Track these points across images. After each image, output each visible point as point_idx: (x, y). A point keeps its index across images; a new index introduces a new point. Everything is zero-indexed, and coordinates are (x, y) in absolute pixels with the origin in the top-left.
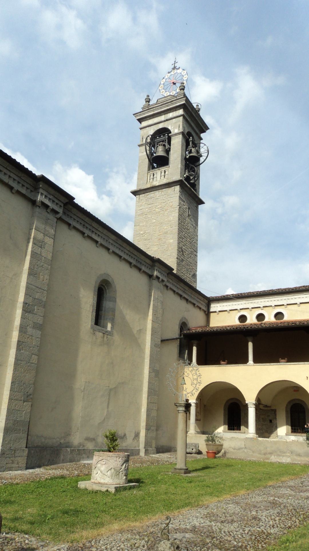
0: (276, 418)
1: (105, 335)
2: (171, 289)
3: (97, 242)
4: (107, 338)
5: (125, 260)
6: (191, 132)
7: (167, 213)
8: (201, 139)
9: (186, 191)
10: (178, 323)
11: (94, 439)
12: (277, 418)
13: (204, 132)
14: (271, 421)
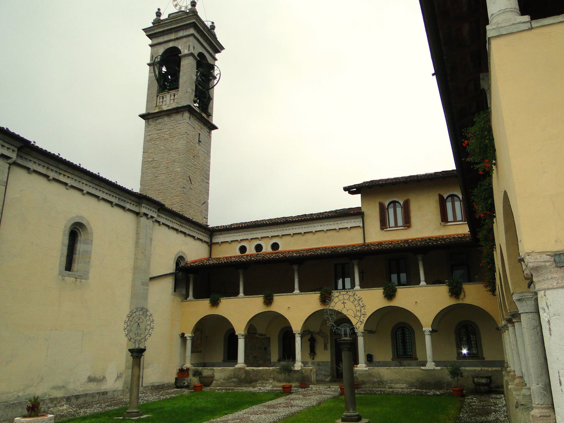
1: (77, 279)
2: (163, 224)
3: (66, 184)
4: (81, 282)
5: (103, 199)
6: (203, 52)
7: (175, 140)
9: (195, 116)
10: (173, 258)
11: (64, 387)
13: (219, 52)
14: (265, 349)
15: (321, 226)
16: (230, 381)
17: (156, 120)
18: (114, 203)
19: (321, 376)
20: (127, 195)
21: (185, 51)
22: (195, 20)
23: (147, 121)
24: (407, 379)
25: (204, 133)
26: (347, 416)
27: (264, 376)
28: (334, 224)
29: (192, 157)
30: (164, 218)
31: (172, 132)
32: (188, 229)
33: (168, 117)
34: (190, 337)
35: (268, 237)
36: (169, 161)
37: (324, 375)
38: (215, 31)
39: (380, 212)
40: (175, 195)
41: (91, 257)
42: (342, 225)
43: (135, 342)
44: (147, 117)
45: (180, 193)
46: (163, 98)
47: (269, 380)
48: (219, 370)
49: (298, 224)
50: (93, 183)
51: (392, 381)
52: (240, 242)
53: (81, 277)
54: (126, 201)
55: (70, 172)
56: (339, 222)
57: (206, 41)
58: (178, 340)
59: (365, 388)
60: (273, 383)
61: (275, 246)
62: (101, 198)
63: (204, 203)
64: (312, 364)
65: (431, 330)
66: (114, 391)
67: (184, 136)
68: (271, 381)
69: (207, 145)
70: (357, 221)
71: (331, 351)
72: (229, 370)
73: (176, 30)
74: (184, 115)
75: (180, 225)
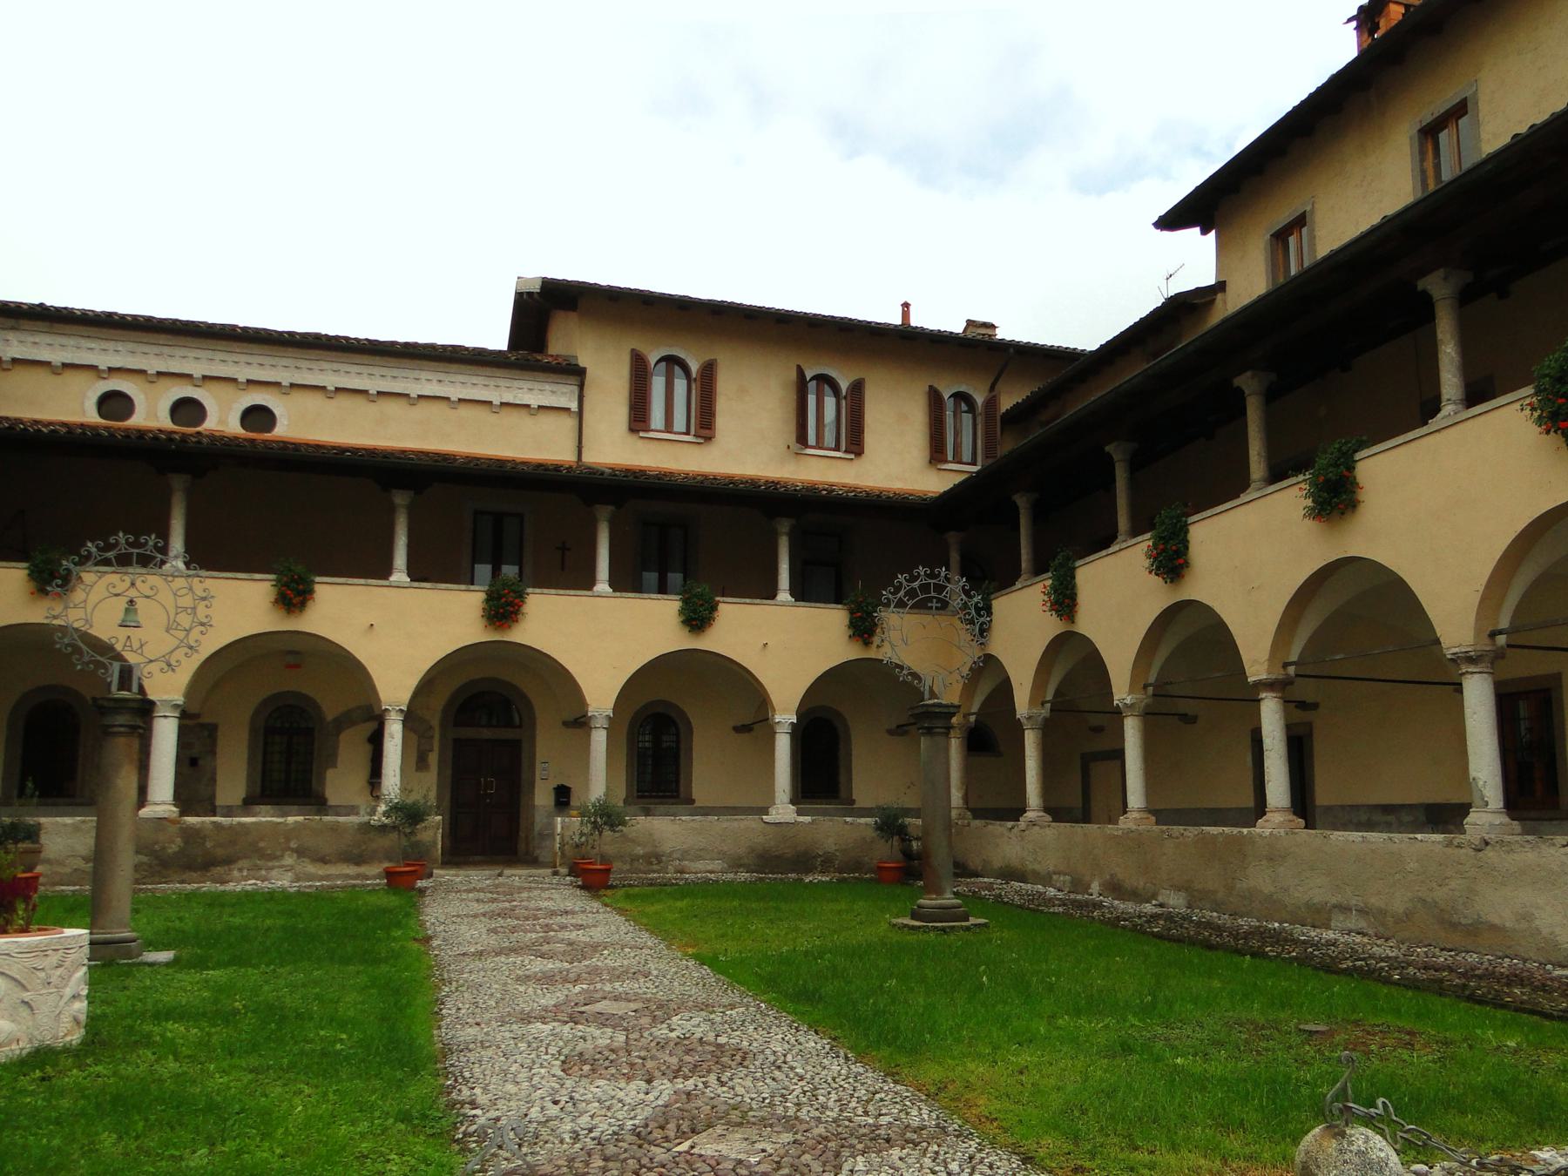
0: (213, 752)
12: (218, 750)
15: (440, 381)
24: (725, 848)
27: (262, 844)
39: (631, 379)
47: (282, 856)
51: (685, 855)
52: (105, 376)
56: (502, 382)
61: (258, 416)
65: (795, 721)
68: (289, 860)
70: (562, 393)
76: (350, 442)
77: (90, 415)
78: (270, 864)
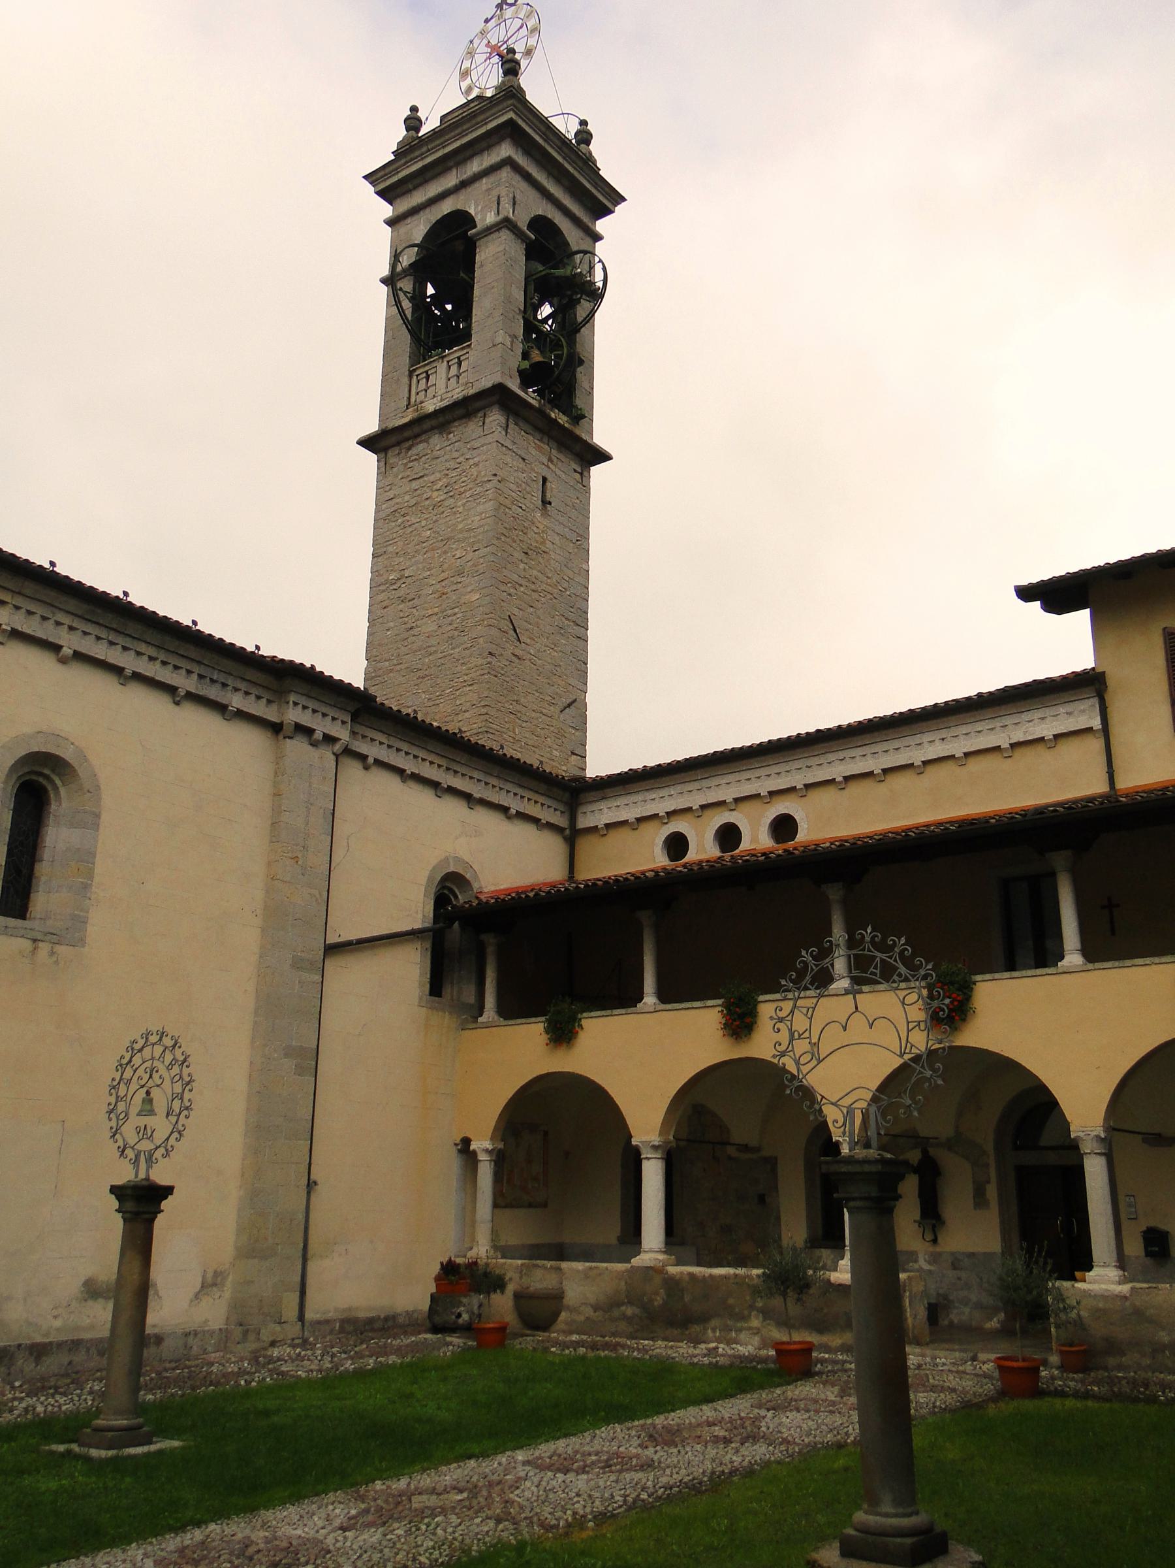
1: (41, 944)
2: (379, 763)
4: (52, 953)
5: (138, 677)
7: (464, 505)
8: (597, 237)
9: (527, 421)
10: (424, 881)
14: (762, 1199)
15: (943, 739)
16: (616, 1313)
17: (409, 449)
18: (182, 692)
19: (967, 1310)
20: (228, 664)
21: (486, 217)
22: (511, 115)
23: (383, 455)
25: (559, 472)
26: (864, 1530)
27: (731, 1301)
28: (992, 729)
29: (518, 555)
30: (381, 743)
31: (454, 480)
32: (479, 780)
33: (441, 433)
34: (487, 1151)
35: (757, 796)
36: (445, 575)
37: (979, 1306)
38: (591, 147)
39: (1168, 666)
40: (465, 681)
41: (92, 870)
42: (1023, 729)
43: (136, 1162)
44: (384, 443)
45: (478, 673)
46: (427, 378)
47: (750, 1316)
48: (578, 1271)
49: (859, 740)
50: (98, 623)
52: (666, 821)
53: (56, 938)
54: (227, 685)
55: (10, 588)
56: (1008, 721)
57: (558, 181)
58: (455, 1163)
59: (1120, 1367)
60: (764, 1331)
61: (784, 827)
62: (128, 672)
63: (569, 705)
64: (929, 1263)
66: (187, 1335)
67: (488, 486)
68: (755, 1323)
69: (574, 514)
71: (1002, 1213)
72: (611, 1272)
73: (459, 158)
74: (487, 421)
75: (448, 769)
76: (1018, 805)
77: (660, 860)
78: (739, 1325)
